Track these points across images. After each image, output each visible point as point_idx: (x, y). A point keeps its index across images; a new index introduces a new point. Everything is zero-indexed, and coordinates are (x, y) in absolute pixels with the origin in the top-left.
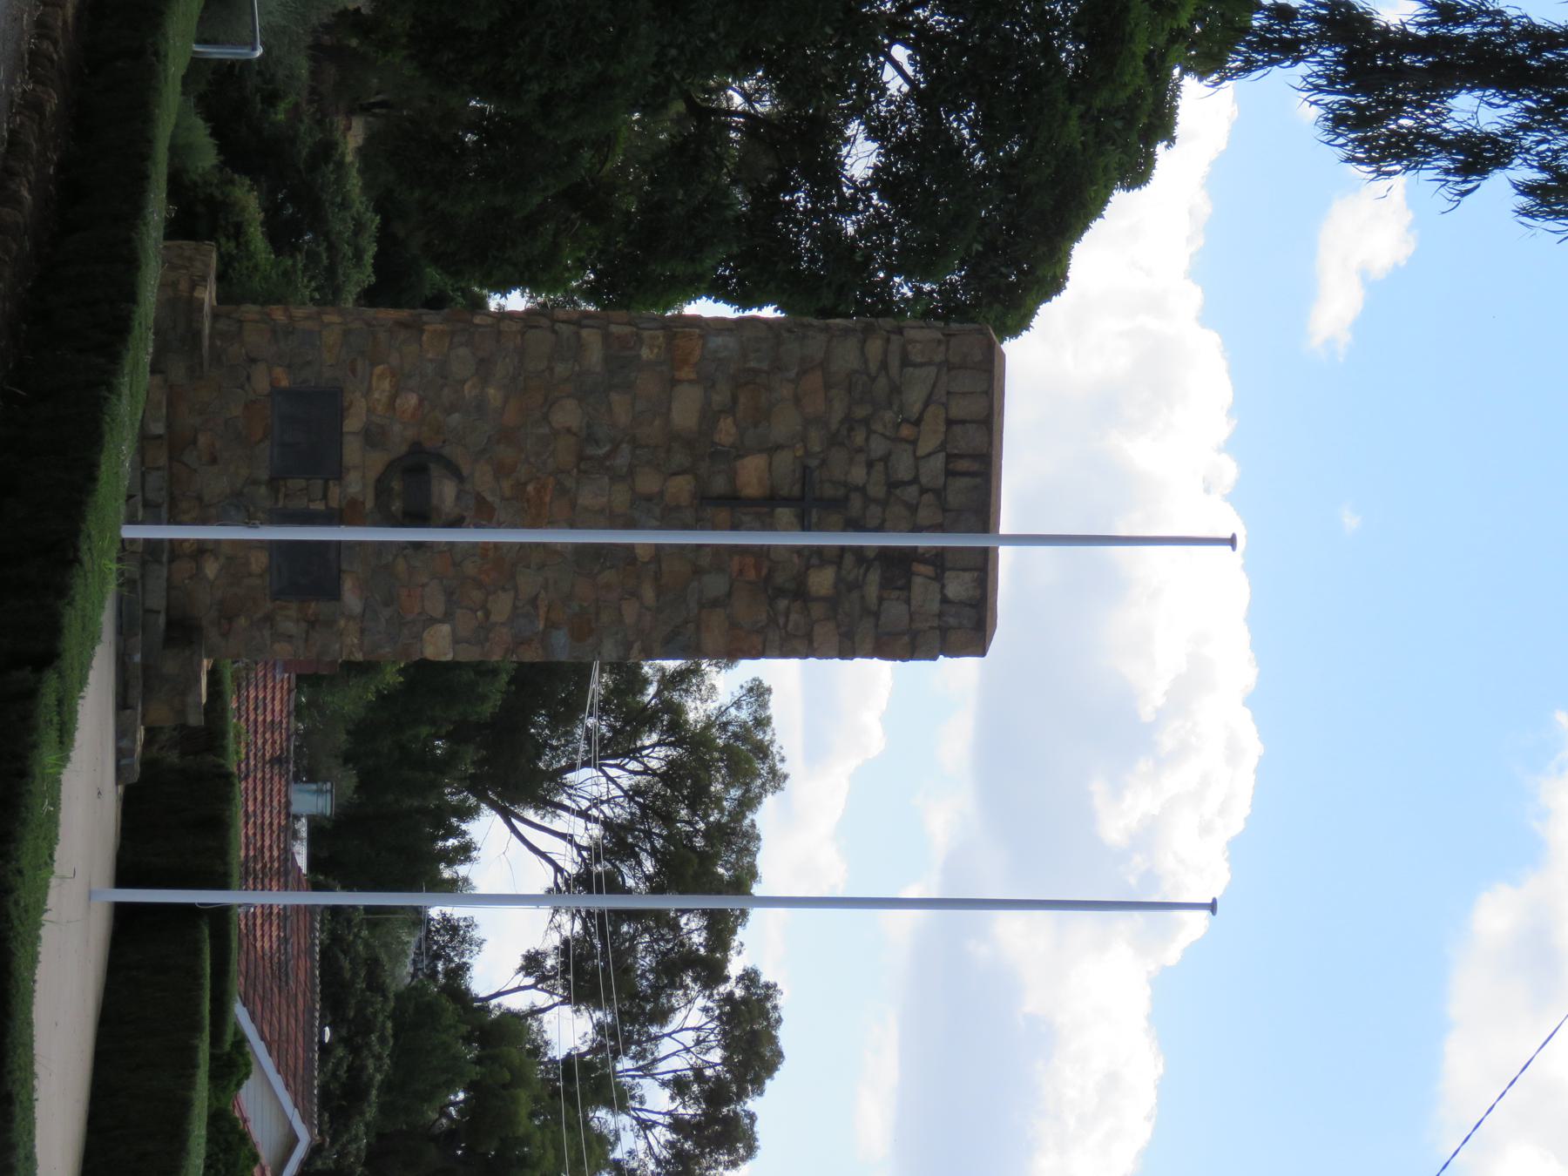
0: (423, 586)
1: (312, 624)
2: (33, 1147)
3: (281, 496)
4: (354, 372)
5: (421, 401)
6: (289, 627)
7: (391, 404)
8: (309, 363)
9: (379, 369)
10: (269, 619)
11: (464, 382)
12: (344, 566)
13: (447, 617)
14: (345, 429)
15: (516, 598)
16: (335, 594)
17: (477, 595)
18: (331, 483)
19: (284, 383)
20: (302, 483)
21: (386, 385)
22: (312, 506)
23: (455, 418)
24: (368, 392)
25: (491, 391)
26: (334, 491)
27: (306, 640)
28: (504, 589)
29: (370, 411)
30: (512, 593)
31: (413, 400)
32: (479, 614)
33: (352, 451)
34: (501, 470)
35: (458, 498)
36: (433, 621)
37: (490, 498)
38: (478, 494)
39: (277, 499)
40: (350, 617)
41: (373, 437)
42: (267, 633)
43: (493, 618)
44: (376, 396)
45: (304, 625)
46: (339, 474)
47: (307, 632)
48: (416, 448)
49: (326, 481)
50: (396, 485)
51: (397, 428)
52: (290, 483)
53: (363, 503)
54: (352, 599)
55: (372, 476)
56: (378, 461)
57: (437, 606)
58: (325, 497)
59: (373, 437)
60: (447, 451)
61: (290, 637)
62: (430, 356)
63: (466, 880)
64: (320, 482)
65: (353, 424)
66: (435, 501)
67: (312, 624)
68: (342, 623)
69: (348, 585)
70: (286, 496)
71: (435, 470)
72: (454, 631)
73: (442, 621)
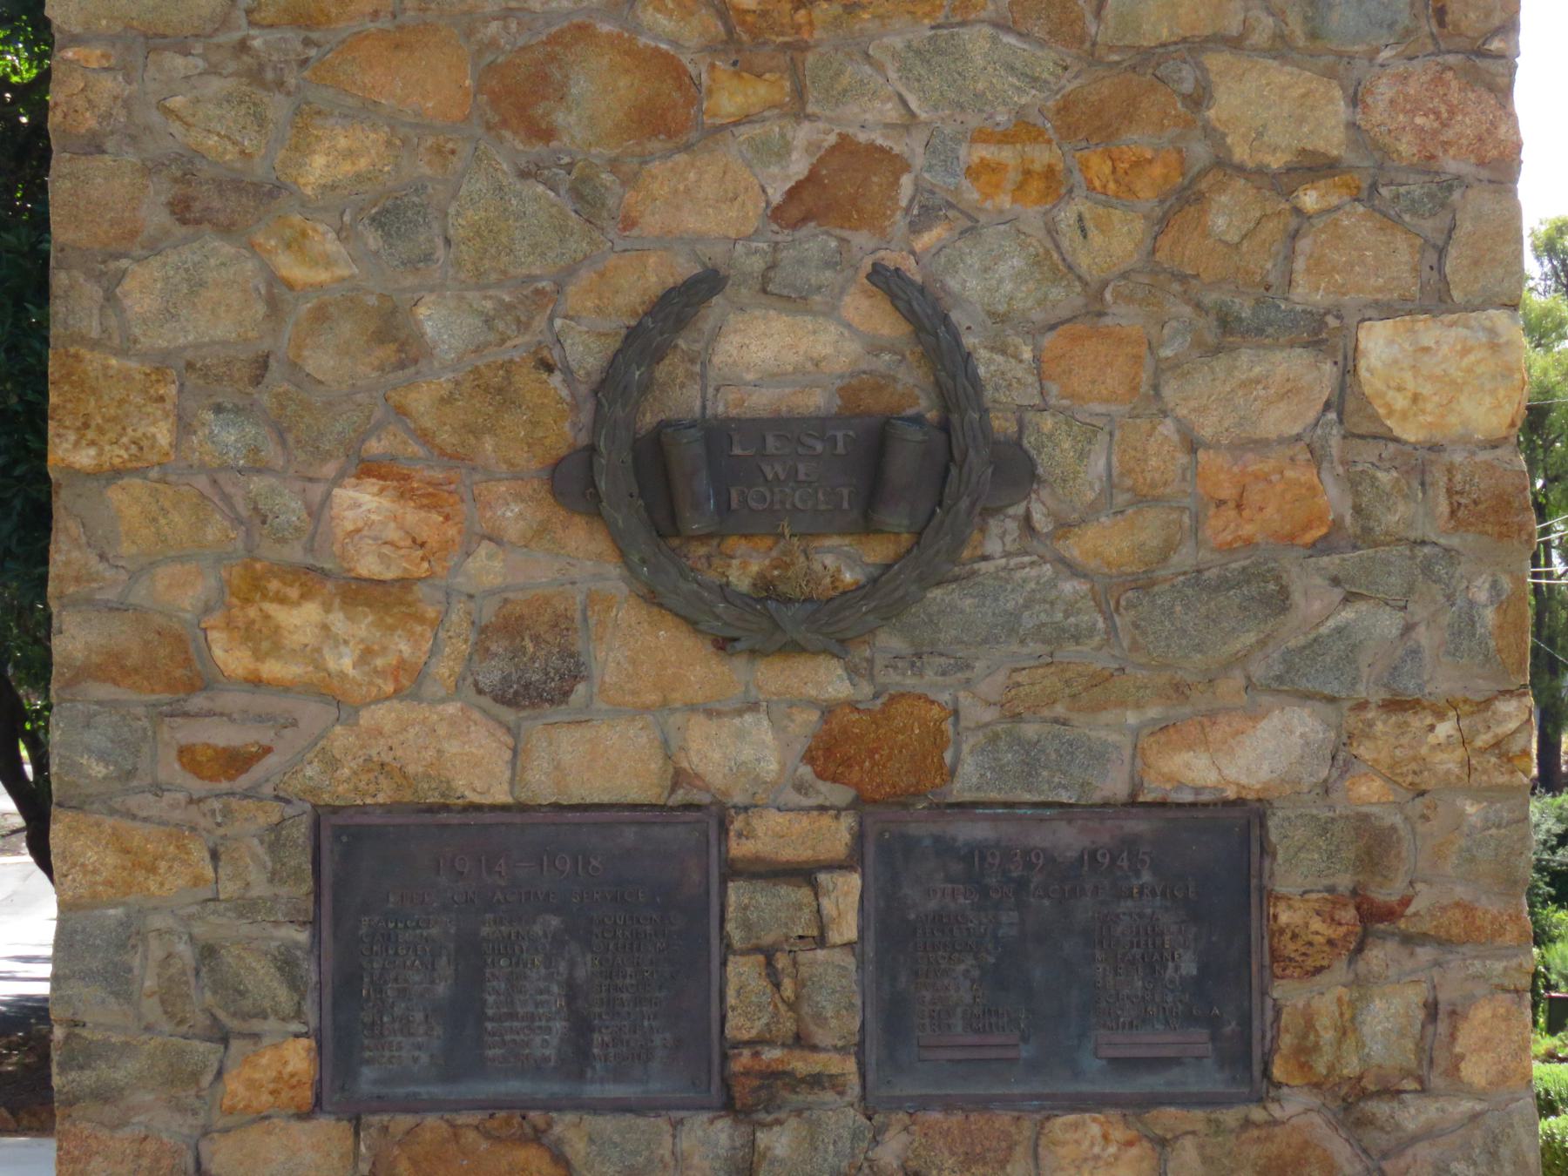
0: (1192, 445)
1: (1373, 918)
2: (1517, 12)
3: (801, 1064)
4: (235, 761)
5: (368, 469)
6: (1388, 1020)
7: (379, 596)
8: (208, 952)
9: (230, 657)
10: (1353, 1102)
11: (277, 295)
12: (1114, 785)
13: (1325, 335)
14: (501, 796)
15: (1235, 43)
16: (1239, 825)
17: (1227, 214)
18: (739, 849)
19: (297, 1058)
20: (743, 973)
21: (300, 619)
22: (847, 929)
23: (440, 323)
24: (336, 699)
25: (317, 168)
26: (769, 835)
27: (1444, 942)
28: (1199, 99)
29: (410, 683)
30: (1215, 61)
31: (361, 503)
32: (1310, 199)
33: (594, 761)
34: (668, 116)
35: (795, 300)
36: (1345, 399)
37: (799, 167)
38: (776, 214)
39: (816, 1081)
40: (1341, 757)
41: (534, 674)
42: (1413, 1115)
43: (1330, 138)
44: (344, 662)
45: (1377, 956)
46: (696, 822)
47: (1409, 940)
48: (573, 483)
49: (733, 870)
50: (745, 566)
51: (486, 569)
52: (740, 1026)
53: (828, 711)
54: (1256, 753)
55: (701, 670)
56: (635, 647)
57: (1275, 390)
58: (804, 874)
59: (534, 674)
60: (586, 351)
61: (1432, 1010)
62: (163, 434)
63: (663, 425)
64: (737, 894)
65: (473, 760)
66: (816, 401)
67: (1373, 918)
68: (1368, 791)
69: (1194, 771)
70: (800, 1041)
71: (680, 397)
72: (1387, 311)
73: (1349, 369)
